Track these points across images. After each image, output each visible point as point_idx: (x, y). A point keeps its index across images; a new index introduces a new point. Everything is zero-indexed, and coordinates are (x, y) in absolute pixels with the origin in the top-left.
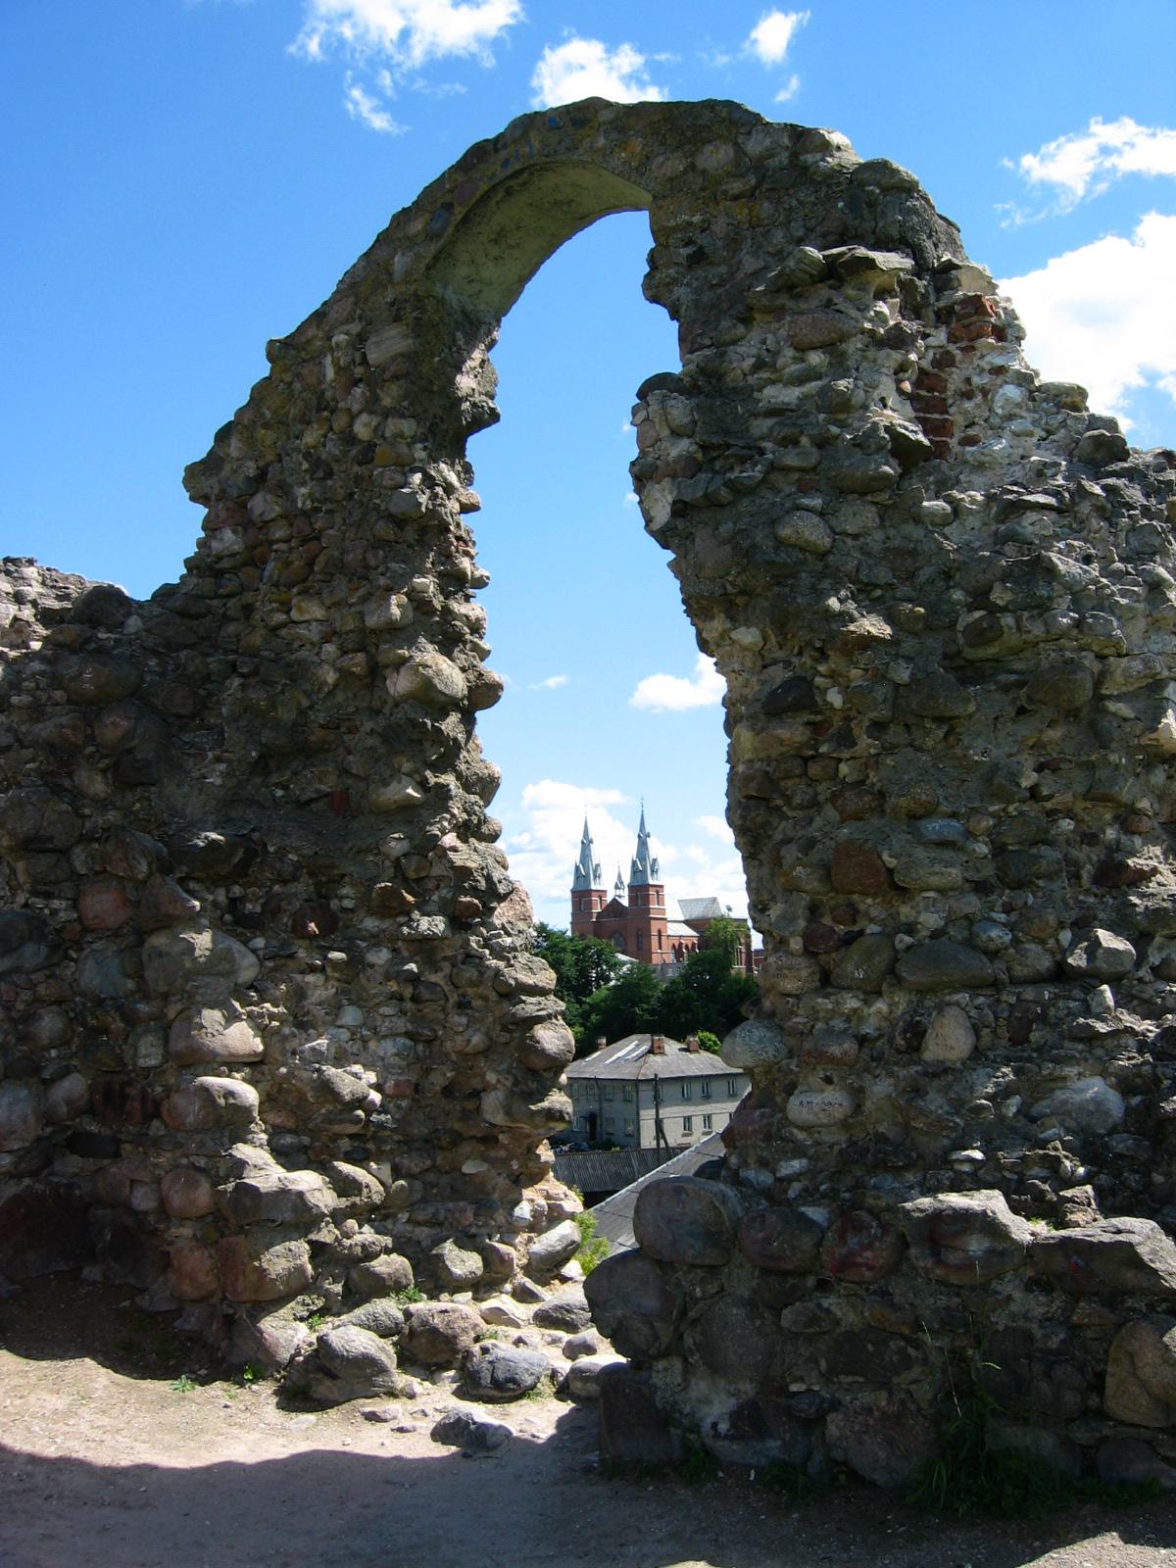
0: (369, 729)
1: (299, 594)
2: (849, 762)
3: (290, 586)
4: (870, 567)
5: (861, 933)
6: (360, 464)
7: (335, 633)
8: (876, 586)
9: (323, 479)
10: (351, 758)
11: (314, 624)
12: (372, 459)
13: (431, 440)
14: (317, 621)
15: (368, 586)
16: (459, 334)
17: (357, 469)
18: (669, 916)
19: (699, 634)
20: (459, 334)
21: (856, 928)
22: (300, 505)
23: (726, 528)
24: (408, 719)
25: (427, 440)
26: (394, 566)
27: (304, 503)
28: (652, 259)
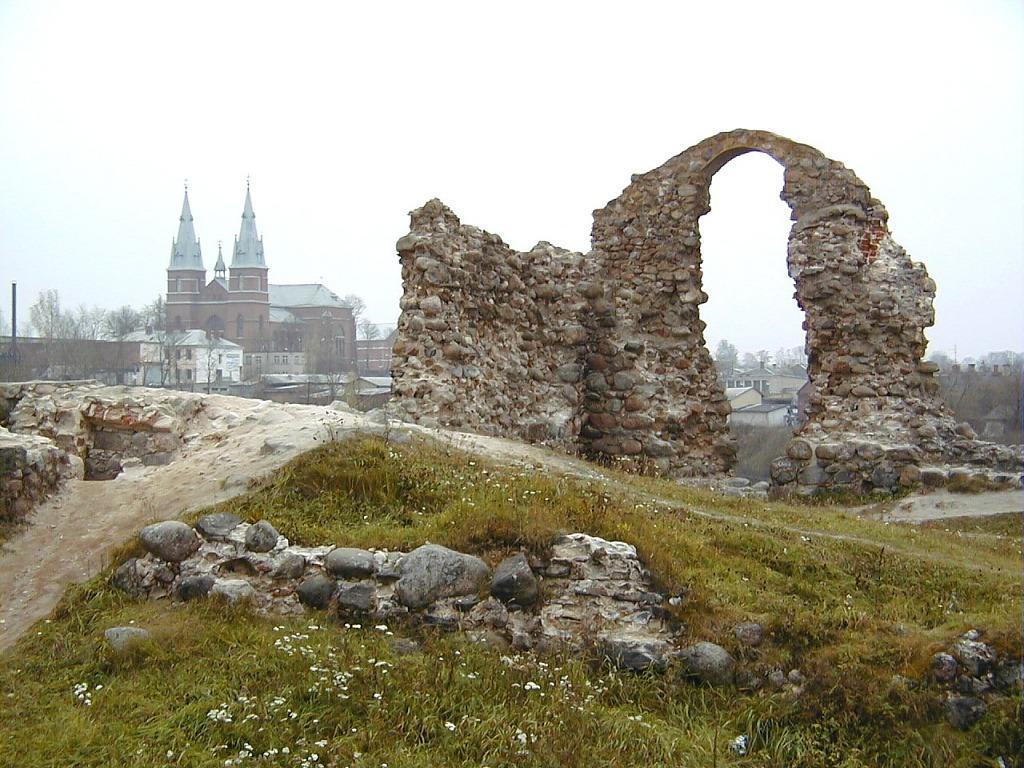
17: (671, 228)
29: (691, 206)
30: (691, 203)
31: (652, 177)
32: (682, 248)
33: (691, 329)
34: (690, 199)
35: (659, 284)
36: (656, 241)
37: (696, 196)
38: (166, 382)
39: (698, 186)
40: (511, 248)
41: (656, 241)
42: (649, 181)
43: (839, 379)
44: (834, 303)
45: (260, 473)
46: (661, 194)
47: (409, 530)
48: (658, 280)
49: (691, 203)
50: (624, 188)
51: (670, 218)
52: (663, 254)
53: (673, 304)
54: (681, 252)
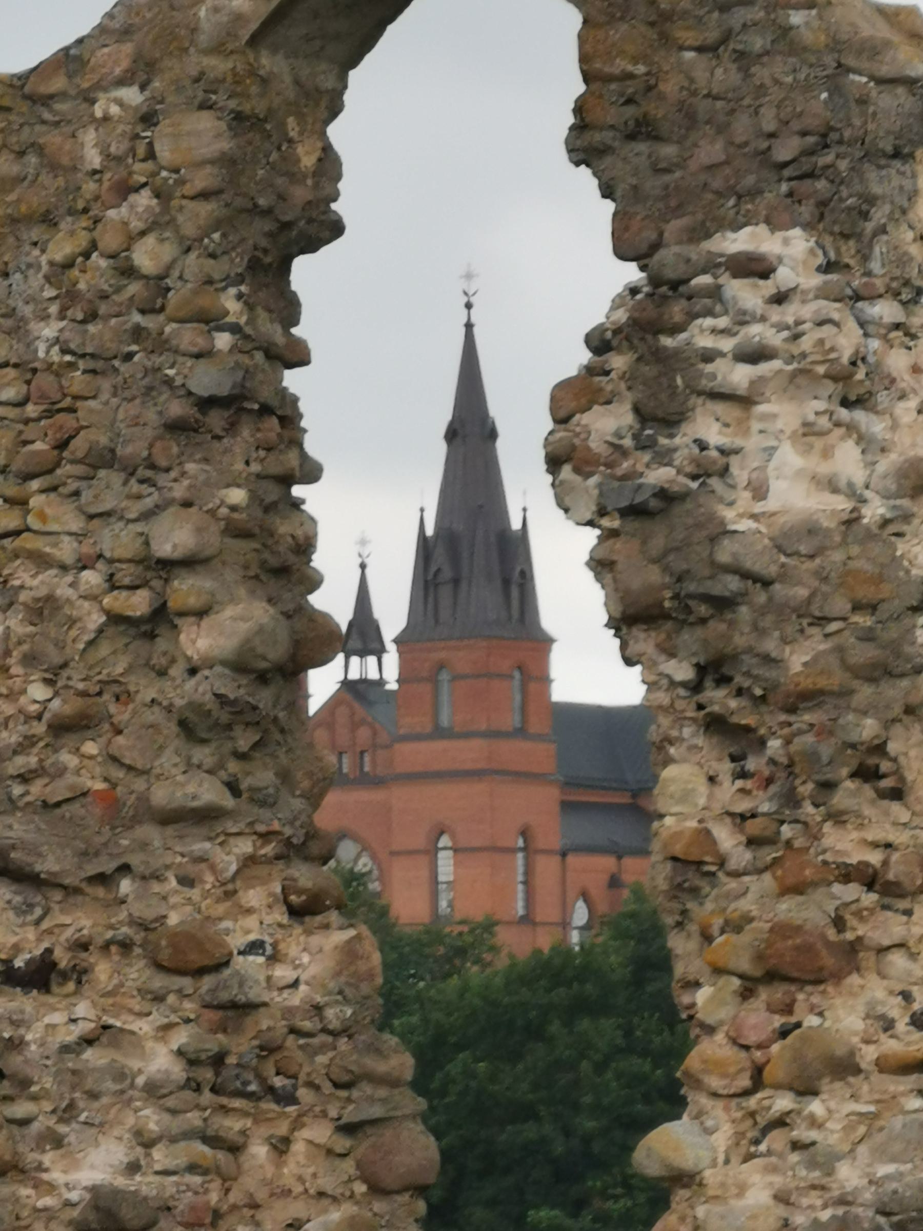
0: (148, 699)
1: (42, 491)
2: (793, 825)
3: (29, 477)
4: (825, 597)
5: (798, 1025)
6: (143, 312)
7: (100, 556)
8: (829, 620)
9: (83, 322)
10: (120, 740)
11: (67, 539)
12: (162, 309)
13: (248, 280)
14: (70, 534)
15: (156, 495)
16: (291, 122)
17: (137, 318)
18: (450, 853)
19: (623, 647)
20: (291, 122)
21: (793, 1020)
22: (41, 354)
23: (658, 543)
24: (215, 695)
25: (241, 282)
26: (191, 467)
27: (48, 352)
28: (579, 109)
29: (206, 209)
30: (204, 195)
31: (58, 83)
32: (177, 409)
33: (233, 788)
34: (201, 180)
35: (92, 578)
36: (77, 380)
37: (226, 161)
38: (445, 720)
39: (239, 117)
40: (292, 379)
41: (77, 380)
42: (46, 100)
43: (788, 1009)
44: (740, 641)
45: (177, 1165)
46: (94, 159)
47: (886, 1130)
48: (84, 564)
49: (204, 195)
50: (597, 193)
51: (129, 272)
52: (104, 440)
53: (162, 673)
54: (176, 427)
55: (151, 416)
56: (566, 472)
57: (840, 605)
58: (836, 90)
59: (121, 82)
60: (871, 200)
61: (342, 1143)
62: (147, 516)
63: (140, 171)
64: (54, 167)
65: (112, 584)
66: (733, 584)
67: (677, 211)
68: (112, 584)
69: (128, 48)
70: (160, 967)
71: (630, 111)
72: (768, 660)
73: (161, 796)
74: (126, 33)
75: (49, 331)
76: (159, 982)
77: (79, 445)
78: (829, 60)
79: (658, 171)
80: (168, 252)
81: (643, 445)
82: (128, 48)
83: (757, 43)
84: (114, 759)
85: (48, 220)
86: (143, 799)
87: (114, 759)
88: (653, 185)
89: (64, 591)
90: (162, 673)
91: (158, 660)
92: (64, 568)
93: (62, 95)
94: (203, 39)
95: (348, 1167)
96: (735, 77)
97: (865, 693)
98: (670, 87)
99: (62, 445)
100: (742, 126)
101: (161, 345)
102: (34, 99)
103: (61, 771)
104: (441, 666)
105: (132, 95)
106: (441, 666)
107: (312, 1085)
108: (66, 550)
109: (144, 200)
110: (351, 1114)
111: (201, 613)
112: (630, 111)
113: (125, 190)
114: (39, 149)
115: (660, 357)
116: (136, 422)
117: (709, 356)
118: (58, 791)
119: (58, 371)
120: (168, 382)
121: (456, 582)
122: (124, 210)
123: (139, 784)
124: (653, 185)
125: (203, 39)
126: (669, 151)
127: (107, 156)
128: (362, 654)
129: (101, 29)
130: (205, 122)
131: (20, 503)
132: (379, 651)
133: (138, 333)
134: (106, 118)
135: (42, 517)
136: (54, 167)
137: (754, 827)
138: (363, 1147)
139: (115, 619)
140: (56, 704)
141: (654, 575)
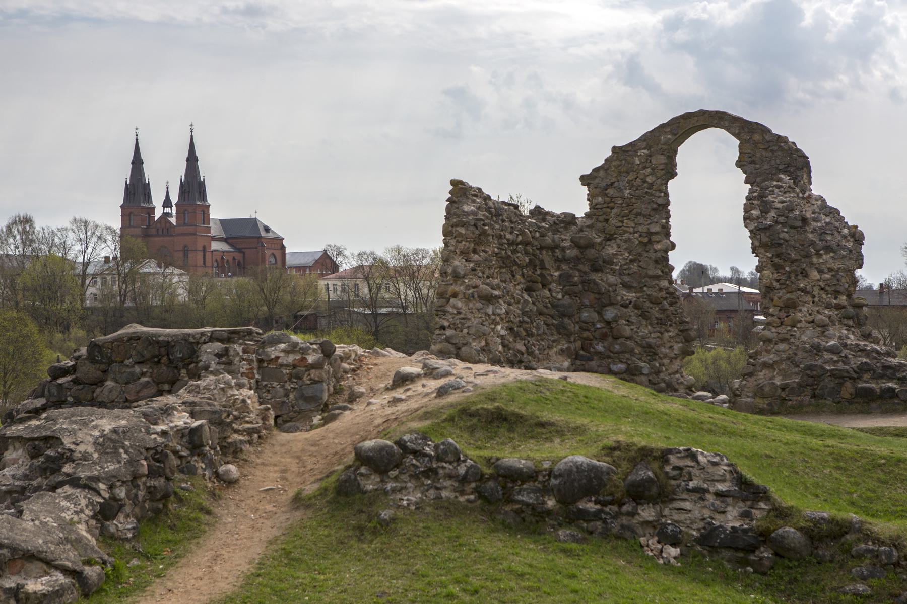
23: (768, 234)
30: (662, 170)
31: (630, 148)
32: (655, 206)
33: (662, 272)
34: (661, 167)
35: (636, 235)
37: (666, 164)
41: (634, 201)
42: (627, 151)
49: (662, 170)
51: (645, 182)
54: (654, 210)
55: (649, 207)
56: (748, 221)
57: (798, 245)
58: (791, 157)
59: (643, 149)
60: (798, 176)
61: (680, 333)
62: (648, 225)
63: (648, 165)
64: (629, 163)
65: (640, 236)
66: (782, 241)
67: (760, 176)
68: (640, 236)
69: (645, 143)
70: (652, 303)
71: (750, 159)
72: (789, 254)
73: (650, 273)
74: (645, 140)
75: (628, 191)
76: (651, 305)
77: (634, 211)
78: (789, 152)
79: (755, 169)
80: (654, 179)
81: (763, 217)
82: (645, 143)
83: (775, 148)
84: (640, 267)
85: (628, 172)
86: (647, 273)
87: (640, 267)
88: (754, 172)
89: (632, 237)
90: (647, 251)
91: (647, 249)
92: (631, 233)
93: (630, 151)
94: (662, 143)
95: (682, 337)
96: (771, 154)
97: (803, 260)
98: (758, 155)
99: (630, 212)
100: (773, 162)
101: (652, 195)
102: (624, 151)
103: (631, 268)
104: (186, 210)
105: (646, 151)
106: (186, 210)
107: (675, 323)
108: (631, 230)
109: (649, 170)
110: (682, 328)
111: (658, 242)
112: (750, 159)
113: (645, 167)
114: (626, 160)
115: (763, 201)
116: (647, 208)
117: (774, 202)
118: (631, 272)
119: (630, 199)
120: (653, 201)
121: (134, 194)
122: (644, 171)
123: (645, 271)
124: (754, 172)
125: (662, 143)
126: (758, 166)
127: (641, 162)
128: (167, 207)
129: (639, 140)
130: (662, 157)
131: (622, 222)
132: (171, 207)
133: (646, 193)
134: (641, 155)
135: (627, 224)
136: (629, 163)
137: (781, 282)
138: (684, 334)
139: (640, 242)
140: (631, 257)
141: (767, 239)
